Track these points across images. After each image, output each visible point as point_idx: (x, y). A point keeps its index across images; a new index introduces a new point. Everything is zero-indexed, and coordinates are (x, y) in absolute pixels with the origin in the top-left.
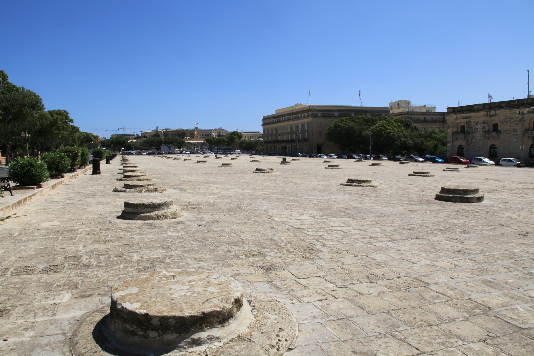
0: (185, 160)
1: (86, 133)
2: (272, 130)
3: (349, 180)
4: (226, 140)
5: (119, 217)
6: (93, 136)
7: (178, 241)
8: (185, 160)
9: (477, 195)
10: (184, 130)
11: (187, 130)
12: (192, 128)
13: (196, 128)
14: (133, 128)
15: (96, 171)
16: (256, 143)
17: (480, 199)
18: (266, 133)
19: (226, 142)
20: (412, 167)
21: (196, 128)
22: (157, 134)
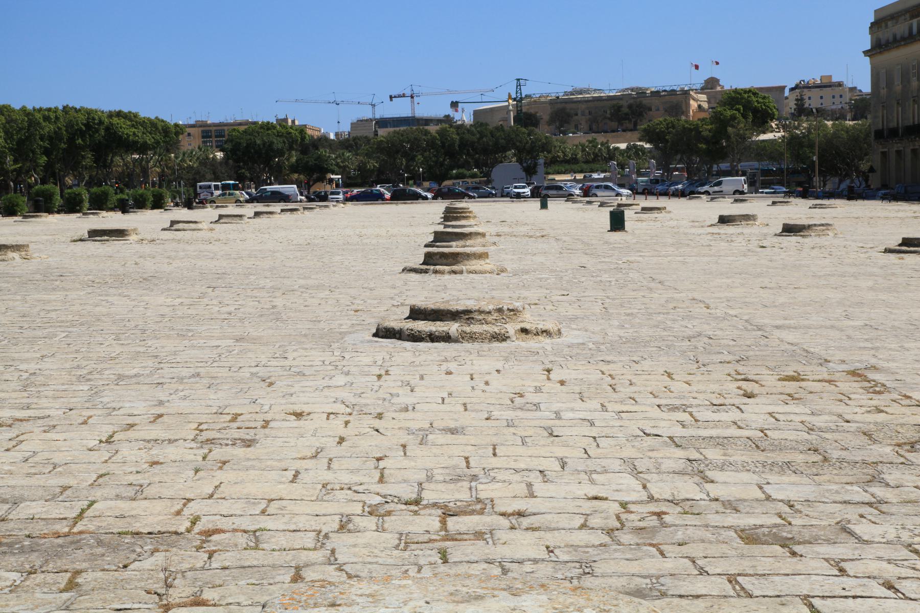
10: (641, 93)
11: (656, 94)
13: (712, 83)
18: (884, 92)
21: (712, 83)
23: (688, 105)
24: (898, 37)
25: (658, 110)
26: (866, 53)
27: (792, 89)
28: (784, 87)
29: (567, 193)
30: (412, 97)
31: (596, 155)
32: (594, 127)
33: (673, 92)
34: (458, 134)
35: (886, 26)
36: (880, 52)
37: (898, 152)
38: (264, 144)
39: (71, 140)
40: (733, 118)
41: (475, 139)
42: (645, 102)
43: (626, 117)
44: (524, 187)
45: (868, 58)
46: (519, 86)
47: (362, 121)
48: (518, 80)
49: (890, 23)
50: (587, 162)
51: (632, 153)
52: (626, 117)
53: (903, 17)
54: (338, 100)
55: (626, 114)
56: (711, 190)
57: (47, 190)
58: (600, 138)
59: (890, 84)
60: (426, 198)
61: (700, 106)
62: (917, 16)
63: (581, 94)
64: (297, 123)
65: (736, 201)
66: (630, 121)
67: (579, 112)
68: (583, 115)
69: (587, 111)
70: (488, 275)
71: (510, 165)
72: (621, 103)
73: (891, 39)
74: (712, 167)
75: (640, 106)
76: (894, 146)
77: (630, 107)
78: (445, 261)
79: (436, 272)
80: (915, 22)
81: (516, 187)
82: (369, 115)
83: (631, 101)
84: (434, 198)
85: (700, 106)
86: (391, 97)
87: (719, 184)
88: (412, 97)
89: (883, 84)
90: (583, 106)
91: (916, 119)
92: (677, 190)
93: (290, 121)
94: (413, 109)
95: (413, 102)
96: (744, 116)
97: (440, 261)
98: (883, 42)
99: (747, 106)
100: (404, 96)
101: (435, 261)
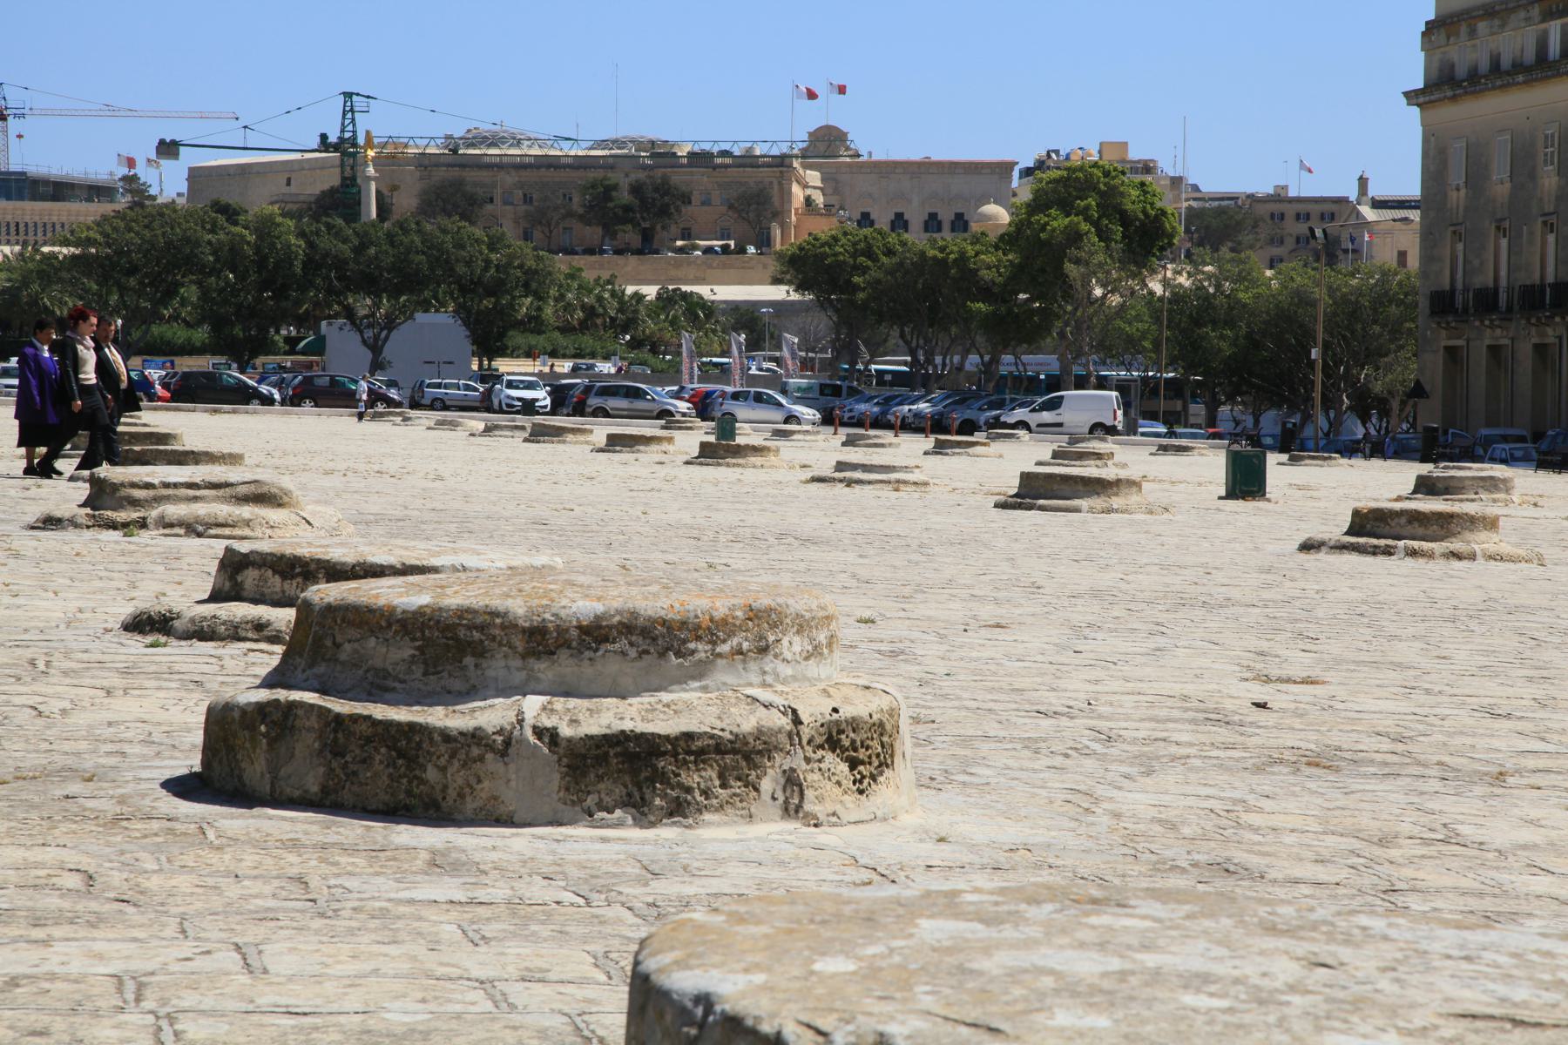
2: (1523, 162)
4: (992, 266)
5: (182, 787)
7: (999, 806)
9: (815, 689)
10: (662, 155)
13: (827, 142)
14: (111, 111)
15: (1246, 482)
16: (1364, 324)
17: (860, 748)
18: (1457, 197)
19: (986, 293)
20: (149, 639)
21: (827, 142)
23: (786, 195)
24: (1506, 63)
25: (706, 203)
26: (1411, 96)
27: (1028, 172)
29: (656, 408)
31: (590, 312)
33: (748, 160)
34: (301, 234)
35: (1473, 33)
36: (1454, 98)
37: (1494, 350)
40: (1075, 237)
41: (345, 250)
42: (678, 178)
43: (626, 215)
44: (530, 386)
45: (1416, 110)
46: (349, 111)
49: (1482, 26)
50: (566, 329)
51: (678, 310)
52: (626, 215)
53: (1522, 14)
55: (627, 208)
56: (1034, 419)
58: (591, 269)
59: (1476, 175)
60: (268, 401)
61: (808, 201)
62: (1561, 14)
63: (493, 145)
65: (1164, 449)
66: (636, 225)
70: (1523, 565)
71: (437, 327)
72: (614, 177)
73: (1484, 66)
74: (995, 361)
75: (664, 188)
76: (1483, 337)
77: (636, 189)
78: (1420, 531)
79: (1413, 553)
80: (1555, 29)
83: (642, 175)
85: (808, 201)
87: (1054, 405)
89: (1456, 175)
90: (510, 179)
91: (1550, 269)
92: (917, 415)
96: (1103, 235)
97: (1409, 530)
98: (1461, 72)
99: (1110, 203)
101: (1398, 530)
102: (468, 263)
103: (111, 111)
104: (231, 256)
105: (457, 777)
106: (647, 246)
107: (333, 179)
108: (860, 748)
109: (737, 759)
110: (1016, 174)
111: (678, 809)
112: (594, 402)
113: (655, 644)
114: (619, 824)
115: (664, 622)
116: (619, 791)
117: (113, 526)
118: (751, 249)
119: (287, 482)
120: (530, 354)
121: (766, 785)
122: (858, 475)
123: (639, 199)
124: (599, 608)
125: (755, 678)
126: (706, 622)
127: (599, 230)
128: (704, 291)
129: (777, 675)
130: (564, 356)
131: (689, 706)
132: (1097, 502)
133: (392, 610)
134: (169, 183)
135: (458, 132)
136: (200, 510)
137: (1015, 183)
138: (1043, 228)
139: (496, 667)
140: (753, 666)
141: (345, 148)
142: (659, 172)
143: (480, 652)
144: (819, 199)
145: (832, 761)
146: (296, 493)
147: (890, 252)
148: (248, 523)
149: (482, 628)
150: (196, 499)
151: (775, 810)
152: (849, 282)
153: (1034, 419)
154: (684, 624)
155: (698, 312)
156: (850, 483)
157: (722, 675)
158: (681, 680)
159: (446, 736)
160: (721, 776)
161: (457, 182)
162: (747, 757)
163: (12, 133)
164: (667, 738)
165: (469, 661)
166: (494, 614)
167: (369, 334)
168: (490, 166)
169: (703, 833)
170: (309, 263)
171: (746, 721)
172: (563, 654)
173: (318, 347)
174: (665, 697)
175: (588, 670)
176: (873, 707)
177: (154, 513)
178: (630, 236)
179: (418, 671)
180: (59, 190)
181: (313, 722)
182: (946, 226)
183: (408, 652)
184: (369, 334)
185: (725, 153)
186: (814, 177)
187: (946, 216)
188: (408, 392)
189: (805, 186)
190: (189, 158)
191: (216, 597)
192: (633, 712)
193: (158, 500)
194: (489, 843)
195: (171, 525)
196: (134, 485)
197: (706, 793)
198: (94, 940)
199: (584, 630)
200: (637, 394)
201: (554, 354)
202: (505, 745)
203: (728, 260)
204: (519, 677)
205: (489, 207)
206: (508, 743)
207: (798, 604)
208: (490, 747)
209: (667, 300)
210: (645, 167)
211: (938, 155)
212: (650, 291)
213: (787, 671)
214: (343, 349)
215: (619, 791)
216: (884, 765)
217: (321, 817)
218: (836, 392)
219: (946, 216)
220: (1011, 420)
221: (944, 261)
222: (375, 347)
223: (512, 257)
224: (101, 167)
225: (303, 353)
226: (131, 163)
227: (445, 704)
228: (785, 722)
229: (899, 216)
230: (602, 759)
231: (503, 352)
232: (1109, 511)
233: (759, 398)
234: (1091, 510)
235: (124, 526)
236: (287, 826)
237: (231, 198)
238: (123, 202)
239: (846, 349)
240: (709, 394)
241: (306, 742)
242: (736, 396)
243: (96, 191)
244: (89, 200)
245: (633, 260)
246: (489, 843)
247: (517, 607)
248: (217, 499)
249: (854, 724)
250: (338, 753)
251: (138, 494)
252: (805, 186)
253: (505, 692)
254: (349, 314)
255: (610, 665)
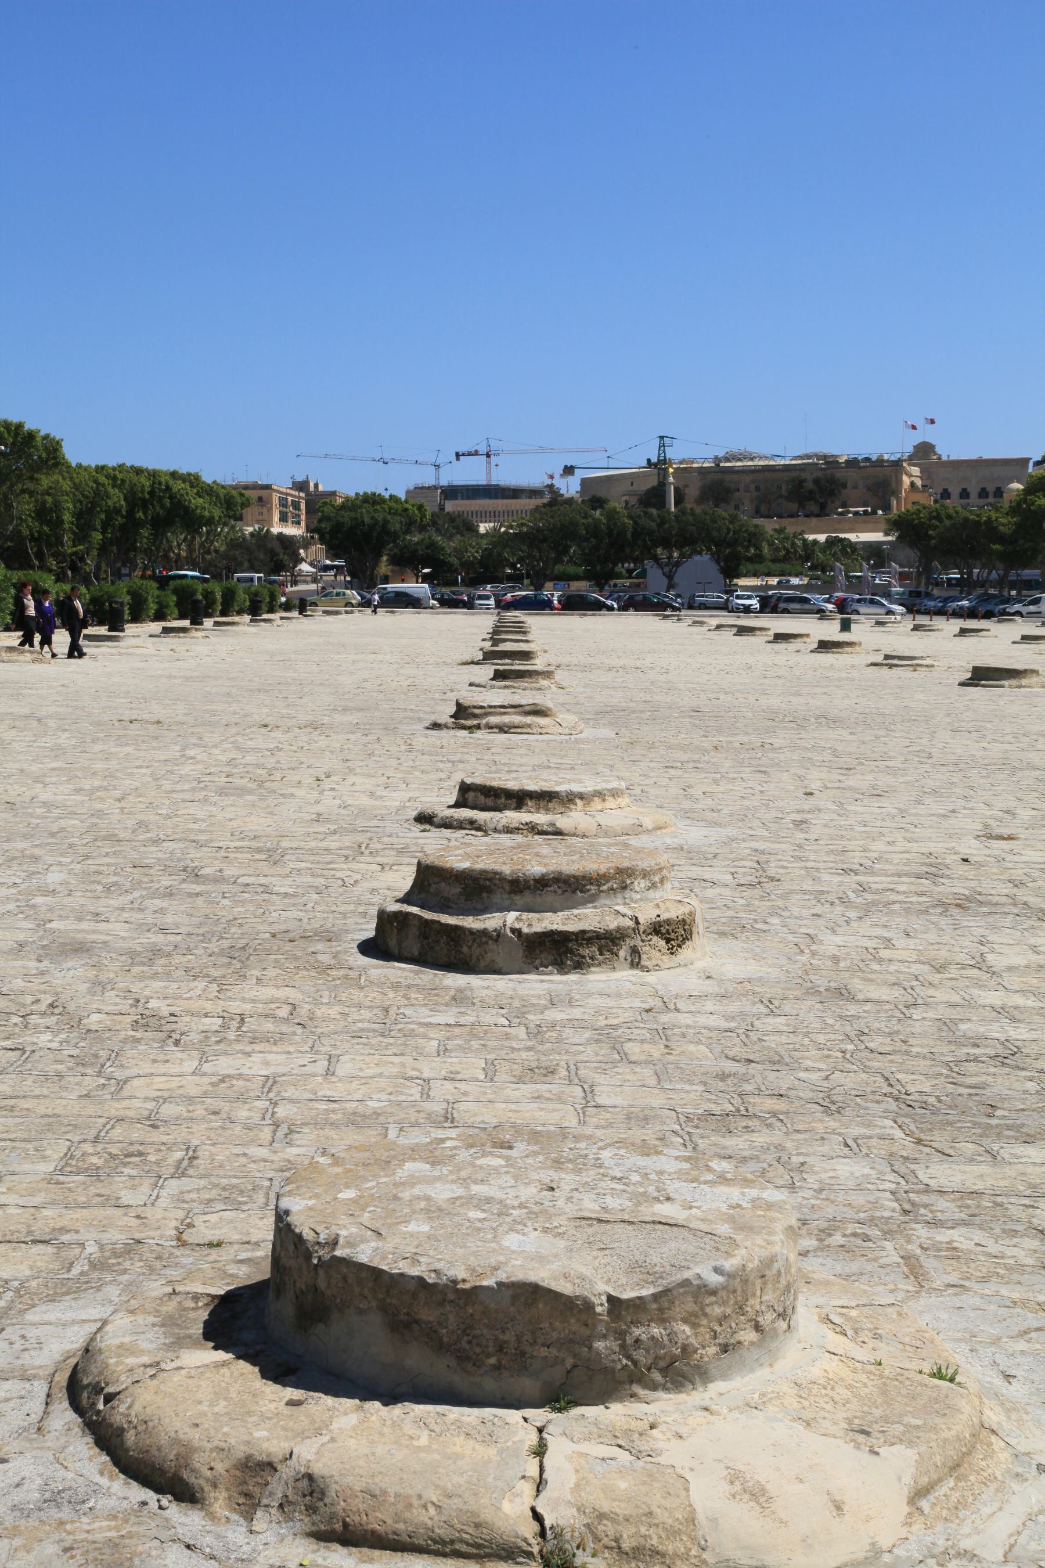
0: (891, 661)
1: (154, 474)
3: (465, 789)
4: (1006, 523)
6: (209, 491)
8: (891, 661)
9: (646, 906)
10: (831, 462)
11: (852, 463)
12: (893, 445)
13: (924, 450)
14: (542, 450)
17: (673, 934)
19: (1001, 539)
20: (423, 827)
21: (924, 450)
22: (653, 488)
23: (900, 482)
25: (855, 487)
28: (1027, 460)
29: (815, 608)
30: (488, 456)
32: (763, 509)
33: (880, 462)
34: (630, 517)
38: (376, 523)
39: (131, 513)
41: (653, 525)
42: (839, 474)
44: (749, 597)
46: (662, 446)
47: (422, 488)
48: (662, 438)
51: (837, 549)
54: (387, 457)
55: (811, 492)
56: (1025, 610)
57: (188, 586)
58: (791, 527)
60: (611, 609)
61: (912, 484)
63: (740, 460)
64: (321, 488)
67: (742, 486)
68: (746, 491)
69: (753, 486)
72: (804, 475)
75: (832, 480)
77: (816, 481)
81: (738, 597)
82: (430, 481)
83: (820, 474)
84: (623, 608)
85: (912, 484)
86: (458, 455)
87: (1036, 602)
88: (488, 456)
90: (748, 478)
92: (961, 608)
93: (312, 485)
94: (489, 473)
95: (489, 463)
100: (476, 453)
102: (719, 530)
103: (542, 450)
104: (594, 530)
105: (476, 951)
106: (823, 512)
107: (654, 482)
108: (673, 934)
109: (607, 943)
110: (1031, 464)
111: (579, 966)
112: (782, 605)
113: (571, 888)
114: (551, 973)
115: (574, 877)
116: (551, 958)
117: (464, 728)
118: (880, 512)
119: (550, 704)
120: (756, 575)
121: (622, 953)
122: (895, 662)
123: (817, 487)
124: (544, 870)
125: (620, 901)
126: (595, 875)
127: (796, 505)
128: (852, 537)
129: (632, 899)
130: (774, 576)
131: (586, 916)
132: (1014, 682)
133: (452, 869)
134: (570, 488)
135: (721, 454)
136: (506, 719)
137: (1030, 470)
138: (1033, 504)
139: (497, 898)
140: (619, 895)
141: (659, 466)
142: (829, 472)
143: (489, 891)
144: (919, 483)
145: (655, 939)
146: (554, 709)
147: (949, 517)
148: (529, 726)
149: (490, 880)
150: (505, 713)
151: (627, 965)
152: (926, 534)
153: (1025, 610)
154: (584, 877)
155: (848, 549)
156: (891, 666)
157: (603, 901)
158: (583, 903)
159: (471, 932)
160: (600, 950)
161: (719, 483)
162: (612, 941)
163: (493, 464)
164: (573, 933)
165: (484, 895)
166: (496, 873)
167: (667, 569)
168: (738, 472)
169: (590, 977)
170: (636, 533)
171: (612, 923)
172: (527, 893)
173: (643, 575)
174: (575, 912)
175: (538, 900)
176: (679, 913)
177: (484, 721)
178: (813, 507)
179: (463, 899)
180: (515, 493)
181: (416, 922)
182: (991, 495)
183: (458, 890)
184: (667, 569)
185: (867, 459)
186: (915, 471)
187: (991, 489)
188: (686, 601)
189: (910, 476)
190: (579, 475)
191: (457, 805)
192: (558, 920)
193: (487, 714)
194: (486, 983)
195: (491, 728)
196: (475, 707)
197: (592, 958)
198: (269, 1052)
199: (536, 881)
200: (806, 601)
201: (769, 575)
202: (497, 936)
203: (865, 521)
204: (507, 903)
205: (737, 494)
206: (498, 935)
207: (642, 864)
208: (491, 937)
209: (831, 542)
210: (822, 469)
211: (987, 455)
212: (822, 538)
213: (638, 896)
214: (655, 580)
215: (551, 958)
216: (685, 939)
217: (417, 968)
218: (918, 594)
219: (991, 489)
220: (1012, 611)
221: (978, 522)
222: (670, 577)
223: (742, 526)
224: (535, 479)
225: (636, 577)
226: (552, 477)
227: (473, 915)
228: (631, 924)
229: (964, 490)
230: (542, 943)
231: (738, 577)
232: (1020, 687)
233: (872, 602)
234: (1010, 687)
235: (469, 728)
236: (399, 973)
237: (601, 494)
238: (546, 499)
239: (926, 571)
240: (845, 600)
241: (413, 931)
242: (859, 601)
243: (533, 493)
244: (530, 497)
245: (814, 521)
246: (486, 983)
247: (506, 870)
248: (515, 713)
249: (668, 922)
250: (426, 938)
251: (477, 711)
252: (910, 476)
253: (501, 910)
254: (656, 559)
255: (549, 897)
